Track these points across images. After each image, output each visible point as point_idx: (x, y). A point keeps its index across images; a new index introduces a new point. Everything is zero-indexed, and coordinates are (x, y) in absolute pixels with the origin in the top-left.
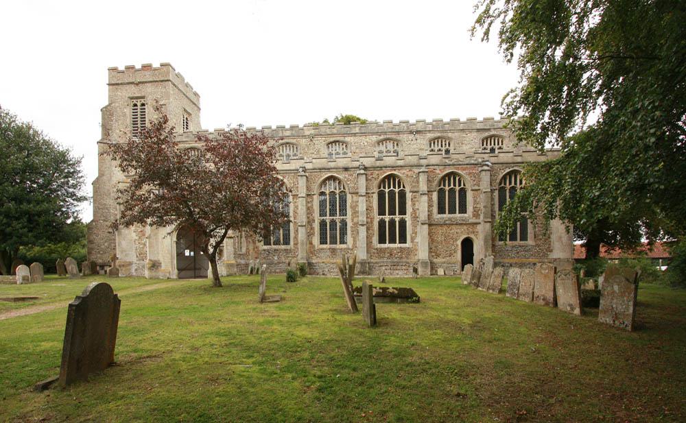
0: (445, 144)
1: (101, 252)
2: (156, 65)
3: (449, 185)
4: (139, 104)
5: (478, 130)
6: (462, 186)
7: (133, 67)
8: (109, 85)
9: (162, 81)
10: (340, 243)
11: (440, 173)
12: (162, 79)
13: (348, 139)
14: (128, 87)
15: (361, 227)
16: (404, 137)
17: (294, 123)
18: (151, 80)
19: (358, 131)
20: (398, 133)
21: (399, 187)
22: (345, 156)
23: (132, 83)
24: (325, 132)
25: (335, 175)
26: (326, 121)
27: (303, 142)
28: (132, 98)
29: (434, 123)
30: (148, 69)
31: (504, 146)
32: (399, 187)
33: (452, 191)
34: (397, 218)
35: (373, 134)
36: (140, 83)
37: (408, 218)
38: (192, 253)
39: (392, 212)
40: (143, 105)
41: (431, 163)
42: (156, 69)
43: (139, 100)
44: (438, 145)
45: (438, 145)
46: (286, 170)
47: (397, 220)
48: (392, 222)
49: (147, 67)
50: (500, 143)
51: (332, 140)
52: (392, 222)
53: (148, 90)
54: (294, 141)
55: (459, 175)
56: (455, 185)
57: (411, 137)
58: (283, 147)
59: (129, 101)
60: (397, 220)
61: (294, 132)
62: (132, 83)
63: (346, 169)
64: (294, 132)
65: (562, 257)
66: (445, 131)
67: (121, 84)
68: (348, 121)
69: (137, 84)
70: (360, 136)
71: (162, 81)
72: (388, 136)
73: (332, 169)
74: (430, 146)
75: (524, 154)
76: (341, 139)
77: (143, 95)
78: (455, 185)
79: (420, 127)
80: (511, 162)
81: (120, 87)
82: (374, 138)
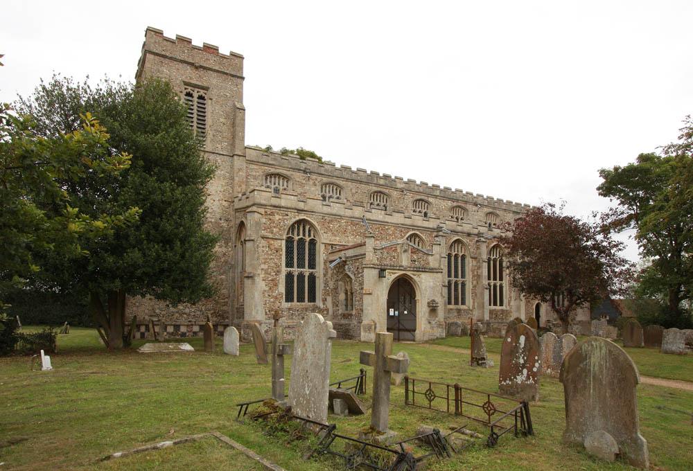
0: (329, 192)
1: (137, 304)
2: (224, 50)
3: (298, 235)
4: (196, 95)
5: (514, 212)
6: (312, 237)
7: (189, 41)
8: (243, 78)
9: (233, 76)
10: (462, 304)
11: (294, 218)
12: (233, 73)
13: (431, 200)
14: (181, 65)
15: (485, 290)
16: (469, 207)
17: (388, 173)
18: (217, 68)
19: (438, 194)
20: (466, 202)
21: (309, 236)
22: (268, 190)
23: (192, 64)
24: (414, 189)
25: (418, 233)
26: (269, 149)
27: (395, 194)
28: (186, 84)
29: (489, 199)
30: (213, 53)
31: (342, 196)
32: (309, 236)
33: (301, 242)
34: (498, 283)
35: (450, 199)
36: (201, 67)
37: (319, 271)
38: (397, 313)
39: (301, 265)
40: (201, 97)
41: (415, 224)
42: (223, 57)
43: (196, 90)
44: (336, 193)
45: (336, 193)
46: (426, 228)
47: (307, 274)
48: (301, 276)
49: (210, 49)
50: (385, 201)
51: (419, 197)
52: (301, 276)
53: (212, 80)
54: (387, 191)
55: (312, 225)
56: (304, 235)
57: (475, 208)
58: (326, 187)
59: (183, 87)
60: (498, 285)
61: (387, 182)
62: (192, 64)
63: (469, 235)
64: (387, 182)
65: (584, 320)
66: (495, 208)
67: (171, 58)
68: (303, 155)
69: (197, 68)
70: (440, 199)
71: (233, 76)
72: (459, 204)
73: (283, 207)
74: (322, 192)
75: (479, 228)
76: (426, 198)
77: (205, 84)
78: (304, 235)
79: (362, 177)
80: (293, 207)
81: (167, 61)
82: (450, 203)
